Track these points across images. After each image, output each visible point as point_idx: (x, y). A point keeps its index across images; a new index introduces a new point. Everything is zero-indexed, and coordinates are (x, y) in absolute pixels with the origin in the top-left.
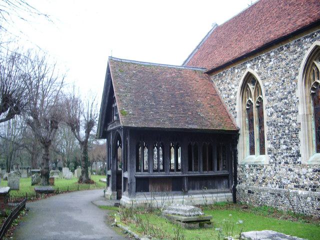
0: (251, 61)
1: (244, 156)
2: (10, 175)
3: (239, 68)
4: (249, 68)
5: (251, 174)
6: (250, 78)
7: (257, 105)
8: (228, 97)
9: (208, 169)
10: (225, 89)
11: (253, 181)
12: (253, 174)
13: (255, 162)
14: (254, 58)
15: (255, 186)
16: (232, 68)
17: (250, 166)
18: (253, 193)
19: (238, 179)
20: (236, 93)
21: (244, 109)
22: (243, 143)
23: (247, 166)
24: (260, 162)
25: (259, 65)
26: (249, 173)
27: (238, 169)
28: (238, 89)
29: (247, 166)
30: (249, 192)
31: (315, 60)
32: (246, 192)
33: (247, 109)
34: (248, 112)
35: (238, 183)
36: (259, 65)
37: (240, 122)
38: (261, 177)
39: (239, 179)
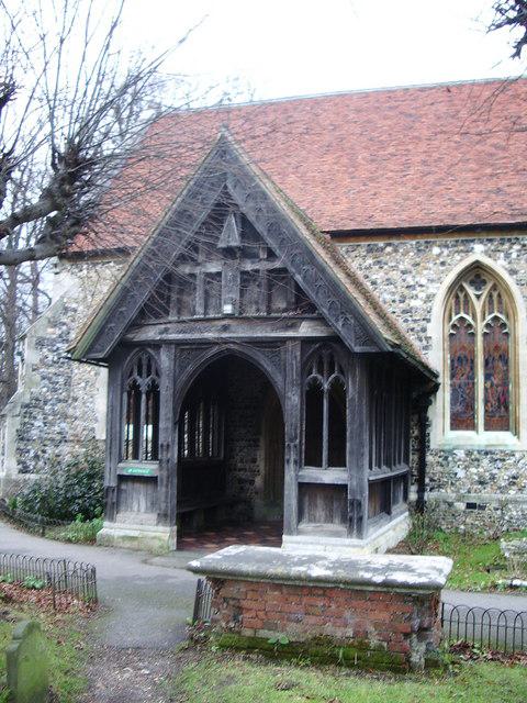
0: (490, 241)
1: (441, 433)
2: (181, 239)
3: (447, 246)
4: (478, 252)
5: (473, 470)
6: (476, 274)
7: (452, 331)
8: (402, 302)
9: (324, 463)
10: (389, 282)
11: (481, 483)
12: (481, 470)
13: (487, 446)
14: (498, 238)
15: (487, 495)
16: (422, 241)
17: (469, 453)
18: (482, 508)
19: (427, 480)
20: (429, 298)
21: (447, 333)
22: (441, 408)
23: (461, 454)
24: (506, 445)
25: (514, 255)
26: (466, 468)
27: (429, 458)
28: (440, 291)
29: (461, 454)
30: (471, 506)
31: (466, 281)
32: (461, 506)
33: (452, 335)
34: (451, 341)
35: (428, 488)
36: (514, 255)
37: (436, 358)
38: (503, 477)
39: (432, 480)
